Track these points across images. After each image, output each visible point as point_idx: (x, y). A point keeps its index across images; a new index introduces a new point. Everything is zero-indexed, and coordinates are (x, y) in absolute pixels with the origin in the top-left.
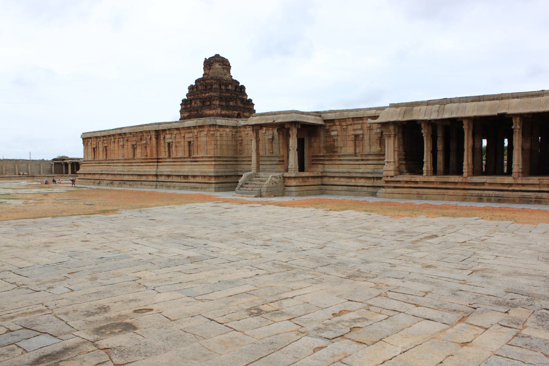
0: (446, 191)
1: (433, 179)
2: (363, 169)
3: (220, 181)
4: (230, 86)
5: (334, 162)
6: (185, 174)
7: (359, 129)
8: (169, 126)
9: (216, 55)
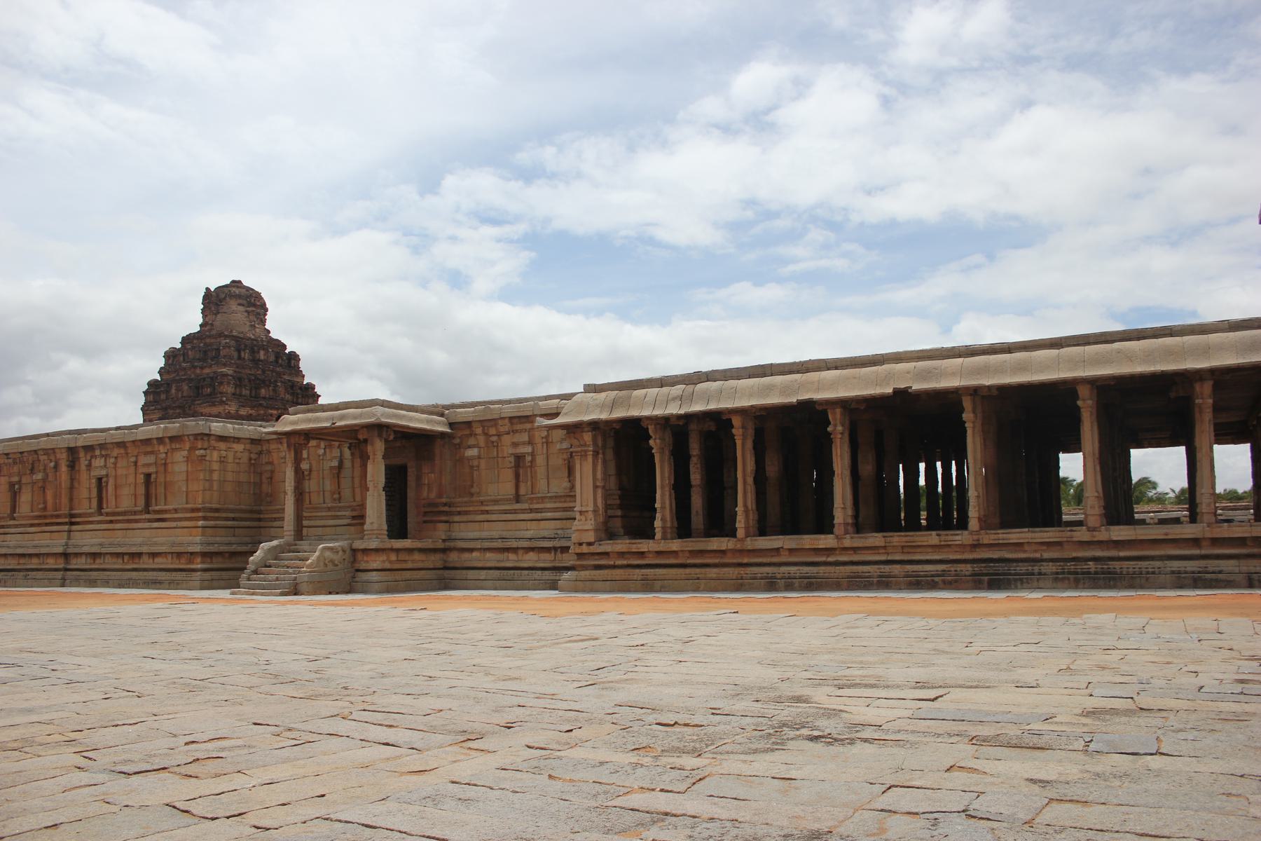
0: (703, 570)
1: (676, 545)
2: (532, 530)
3: (215, 566)
4: (262, 353)
5: (471, 517)
6: (134, 550)
7: (524, 443)
8: (101, 438)
9: (233, 282)
